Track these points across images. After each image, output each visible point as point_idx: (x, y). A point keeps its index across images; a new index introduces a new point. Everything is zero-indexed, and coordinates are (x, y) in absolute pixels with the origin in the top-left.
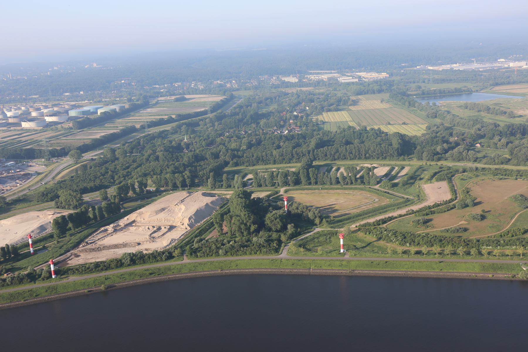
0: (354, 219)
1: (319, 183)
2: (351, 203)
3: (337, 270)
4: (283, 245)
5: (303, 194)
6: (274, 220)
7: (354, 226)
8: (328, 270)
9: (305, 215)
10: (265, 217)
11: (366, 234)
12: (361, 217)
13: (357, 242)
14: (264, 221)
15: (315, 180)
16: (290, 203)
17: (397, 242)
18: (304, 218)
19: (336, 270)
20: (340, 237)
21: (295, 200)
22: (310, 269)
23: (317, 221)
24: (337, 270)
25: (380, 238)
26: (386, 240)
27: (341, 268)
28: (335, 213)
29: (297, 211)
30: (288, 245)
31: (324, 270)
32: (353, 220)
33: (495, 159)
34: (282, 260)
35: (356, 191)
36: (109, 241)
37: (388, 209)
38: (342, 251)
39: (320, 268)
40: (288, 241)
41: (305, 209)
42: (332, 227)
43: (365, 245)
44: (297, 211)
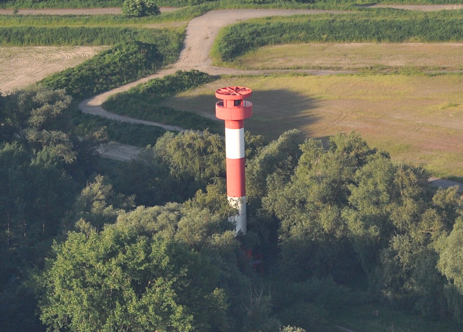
5: (396, 71)
6: (129, 293)
9: (405, 259)
10: (42, 267)
16: (272, 148)
21: (313, 120)
29: (338, 222)
33: (140, 258)
36: (303, 111)
41: (409, 205)
44: (338, 222)
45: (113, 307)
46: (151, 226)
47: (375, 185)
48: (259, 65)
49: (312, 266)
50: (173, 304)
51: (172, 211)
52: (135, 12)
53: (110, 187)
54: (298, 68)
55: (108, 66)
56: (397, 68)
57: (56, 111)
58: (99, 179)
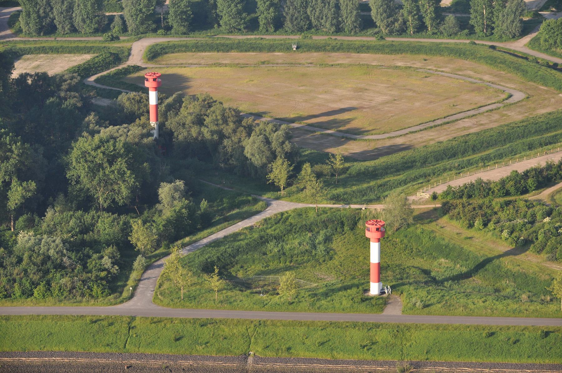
0: (427, 169)
1: (288, 24)
2: (417, 104)
3: (355, 363)
4: (139, 262)
5: (226, 65)
6: (106, 165)
8: (319, 361)
11: (471, 226)
12: (455, 162)
13: (435, 258)
14: (64, 167)
15: (271, 13)
18: (226, 161)
19: (348, 363)
22: (246, 356)
23: (276, 172)
24: (355, 363)
26: (547, 248)
27: (368, 356)
31: (299, 360)
38: (374, 289)
39: (285, 355)
40: (161, 250)
43: (464, 270)
45: (99, 171)
46: (116, 135)
47: (216, 116)
50: (126, 170)
51: (125, 128)
52: (109, 39)
53: (97, 117)
54: (182, 64)
55: (97, 63)
57: (73, 83)
58: (93, 113)
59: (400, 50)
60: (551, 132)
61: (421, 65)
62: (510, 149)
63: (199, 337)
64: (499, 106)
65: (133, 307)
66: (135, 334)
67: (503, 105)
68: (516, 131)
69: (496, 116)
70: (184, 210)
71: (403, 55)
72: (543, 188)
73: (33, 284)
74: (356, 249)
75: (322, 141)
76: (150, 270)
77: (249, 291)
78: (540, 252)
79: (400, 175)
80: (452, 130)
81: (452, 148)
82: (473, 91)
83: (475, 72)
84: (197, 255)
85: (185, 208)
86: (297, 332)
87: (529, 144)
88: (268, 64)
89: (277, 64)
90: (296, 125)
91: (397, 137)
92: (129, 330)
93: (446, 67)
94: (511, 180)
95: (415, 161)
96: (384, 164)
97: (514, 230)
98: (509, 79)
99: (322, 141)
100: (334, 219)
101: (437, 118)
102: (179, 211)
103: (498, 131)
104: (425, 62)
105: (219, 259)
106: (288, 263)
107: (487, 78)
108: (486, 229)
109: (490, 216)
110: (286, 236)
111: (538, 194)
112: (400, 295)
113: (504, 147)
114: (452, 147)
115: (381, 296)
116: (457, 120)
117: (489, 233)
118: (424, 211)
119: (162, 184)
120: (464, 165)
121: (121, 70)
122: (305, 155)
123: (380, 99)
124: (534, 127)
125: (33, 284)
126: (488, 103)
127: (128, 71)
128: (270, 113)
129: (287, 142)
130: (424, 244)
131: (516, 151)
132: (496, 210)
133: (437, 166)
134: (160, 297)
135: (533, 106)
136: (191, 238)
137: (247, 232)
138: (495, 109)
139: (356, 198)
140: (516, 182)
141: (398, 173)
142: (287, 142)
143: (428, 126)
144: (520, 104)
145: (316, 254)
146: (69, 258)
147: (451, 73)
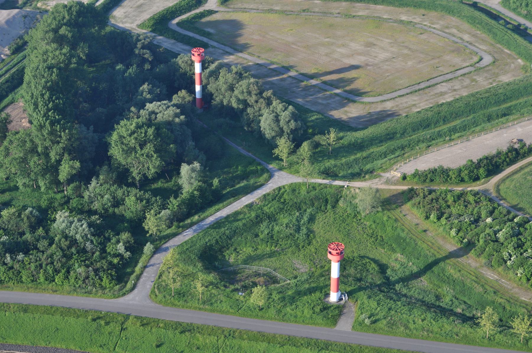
0: (403, 141)
2: (410, 63)
4: (148, 248)
5: (276, 12)
7: (399, 175)
11: (427, 218)
12: (427, 133)
13: (394, 251)
14: (106, 146)
17: (520, 271)
18: (249, 125)
20: (330, 256)
21: (240, 35)
25: (470, 245)
26: (485, 254)
28: (351, 104)
30: (167, 249)
32: (403, 141)
34: (129, 323)
35: (433, 14)
37: (514, 103)
38: (334, 297)
40: (173, 230)
42: (328, 173)
43: (415, 269)
46: (157, 111)
48: (232, 6)
49: (152, 219)
50: (153, 153)
51: (165, 104)
53: (151, 85)
54: (245, 9)
55: (182, 6)
56: (277, 10)
57: (146, 43)
58: (146, 84)
59: (406, 4)
60: (507, 103)
61: (419, 20)
62: (473, 120)
63: (177, 345)
64: (471, 70)
65: (131, 302)
66: (125, 336)
67: (474, 69)
68: (479, 102)
69: (467, 82)
70: (195, 192)
71: (408, 8)
72: (492, 175)
73: (56, 271)
74: (332, 233)
75: (329, 101)
76: (158, 253)
77: (232, 287)
78: (479, 256)
79: (382, 146)
80: (432, 95)
81: (427, 119)
82: (453, 51)
83: (458, 31)
84: (199, 238)
85: (197, 190)
86: (259, 347)
87: (488, 115)
88: (307, 12)
89: (314, 12)
90: (314, 82)
91: (388, 100)
92: (121, 332)
93: (438, 23)
94: (466, 169)
95: (395, 133)
96: (371, 135)
97: (461, 229)
98: (483, 40)
99: (329, 101)
100: (321, 196)
101: (422, 81)
102: (192, 193)
103: (465, 103)
104: (423, 17)
105: (218, 242)
106: (273, 248)
107: (466, 37)
108: (438, 223)
109: (444, 209)
110: (278, 214)
111: (486, 183)
112: (355, 302)
113: (469, 118)
114: (427, 119)
115: (339, 303)
116: (437, 84)
117: (441, 227)
118: (394, 194)
119: (183, 164)
120: (435, 137)
121: (198, 14)
122: (312, 121)
123: (383, 55)
124: (494, 99)
125: (56, 271)
126: (463, 66)
127: (203, 15)
128: (296, 67)
129: (292, 121)
130: (387, 233)
131: (478, 123)
132: (449, 203)
133: (414, 137)
134: (156, 290)
135: (497, 71)
136: (199, 216)
137: (247, 211)
138: (468, 73)
139: (343, 170)
140: (470, 171)
141: (381, 144)
142: (292, 121)
143: (414, 89)
144: (488, 68)
145: (298, 238)
146: (92, 242)
147: (440, 31)
